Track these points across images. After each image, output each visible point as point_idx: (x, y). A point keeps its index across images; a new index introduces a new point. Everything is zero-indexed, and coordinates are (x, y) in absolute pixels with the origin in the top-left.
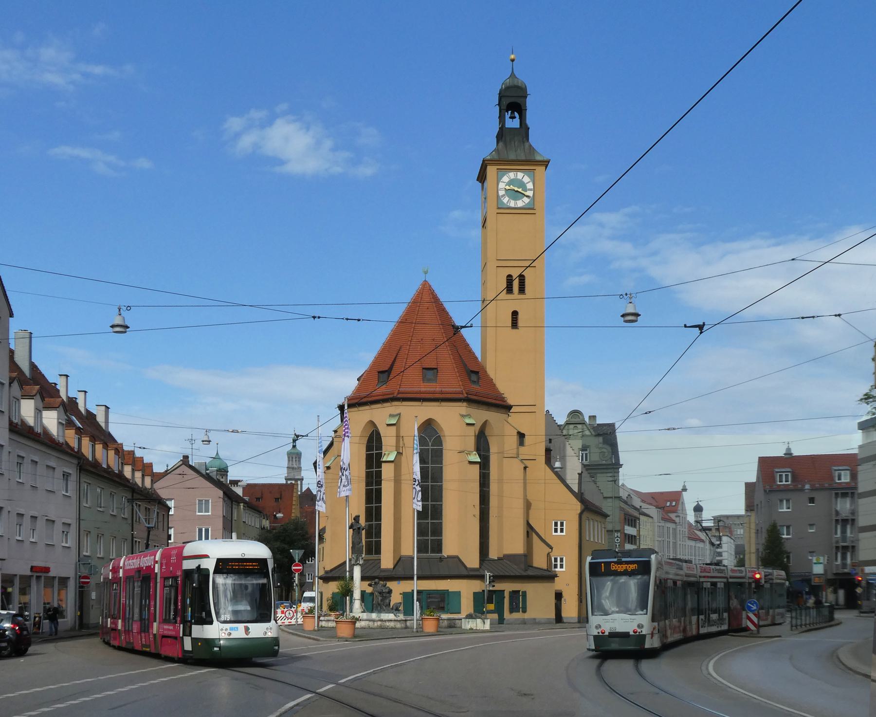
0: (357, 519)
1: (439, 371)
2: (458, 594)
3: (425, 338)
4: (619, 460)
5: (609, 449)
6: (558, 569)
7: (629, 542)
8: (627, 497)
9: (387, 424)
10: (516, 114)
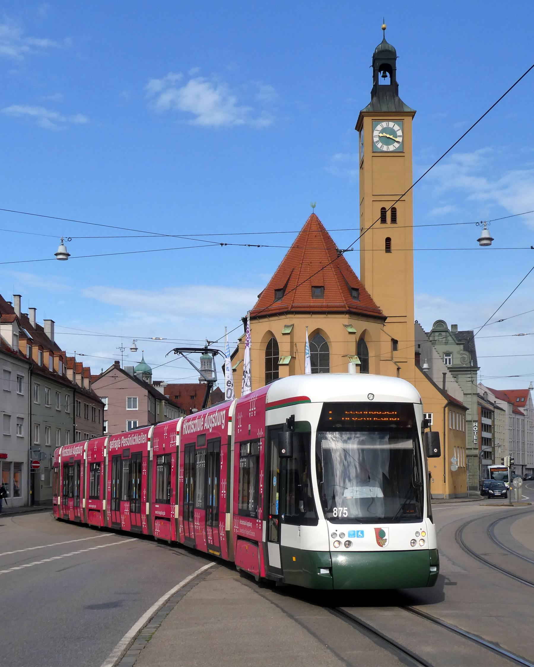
1: (325, 289)
4: (477, 364)
8: (484, 394)
10: (388, 74)
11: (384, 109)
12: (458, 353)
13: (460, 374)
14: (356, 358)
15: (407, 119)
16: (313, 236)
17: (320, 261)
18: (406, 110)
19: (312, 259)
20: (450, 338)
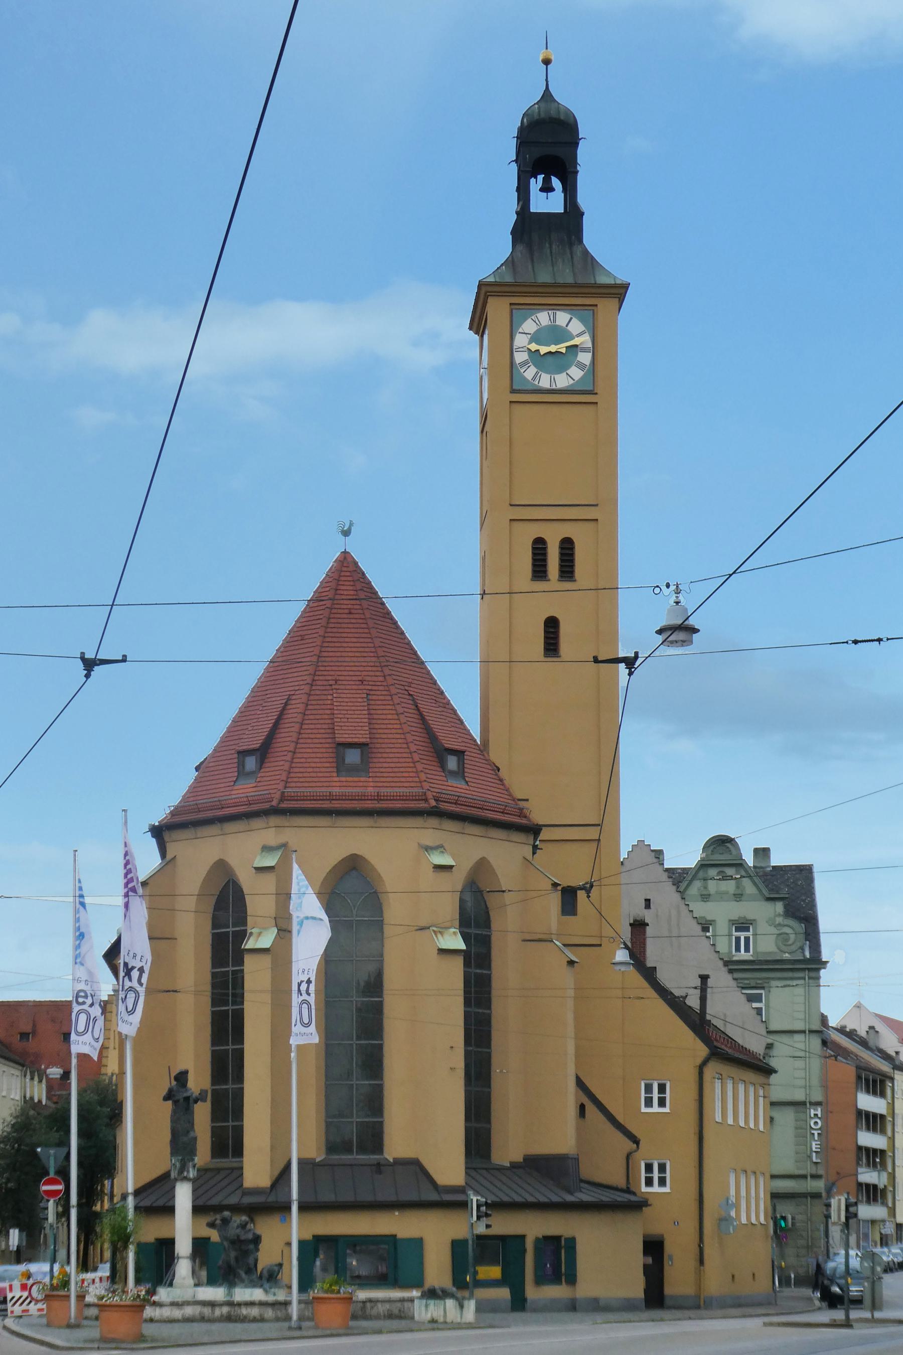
0: (182, 1078)
2: (418, 1244)
3: (341, 678)
4: (819, 952)
5: (800, 927)
7: (868, 1129)
8: (867, 1032)
9: (255, 868)
10: (556, 182)
11: (544, 277)
12: (771, 922)
13: (773, 979)
14: (454, 933)
15: (605, 305)
16: (342, 611)
17: (360, 678)
18: (602, 280)
19: (340, 673)
20: (747, 883)
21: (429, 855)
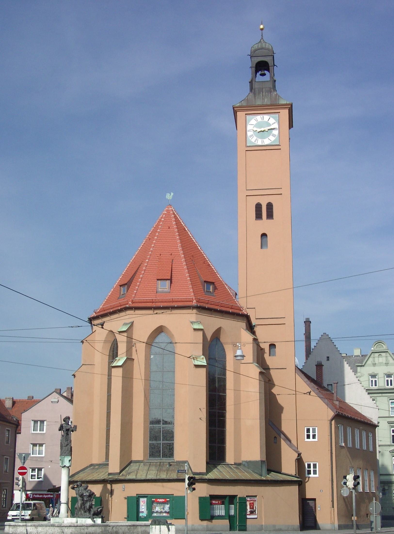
1: (173, 282)
6: (312, 475)
14: (203, 358)
21: (193, 325)
